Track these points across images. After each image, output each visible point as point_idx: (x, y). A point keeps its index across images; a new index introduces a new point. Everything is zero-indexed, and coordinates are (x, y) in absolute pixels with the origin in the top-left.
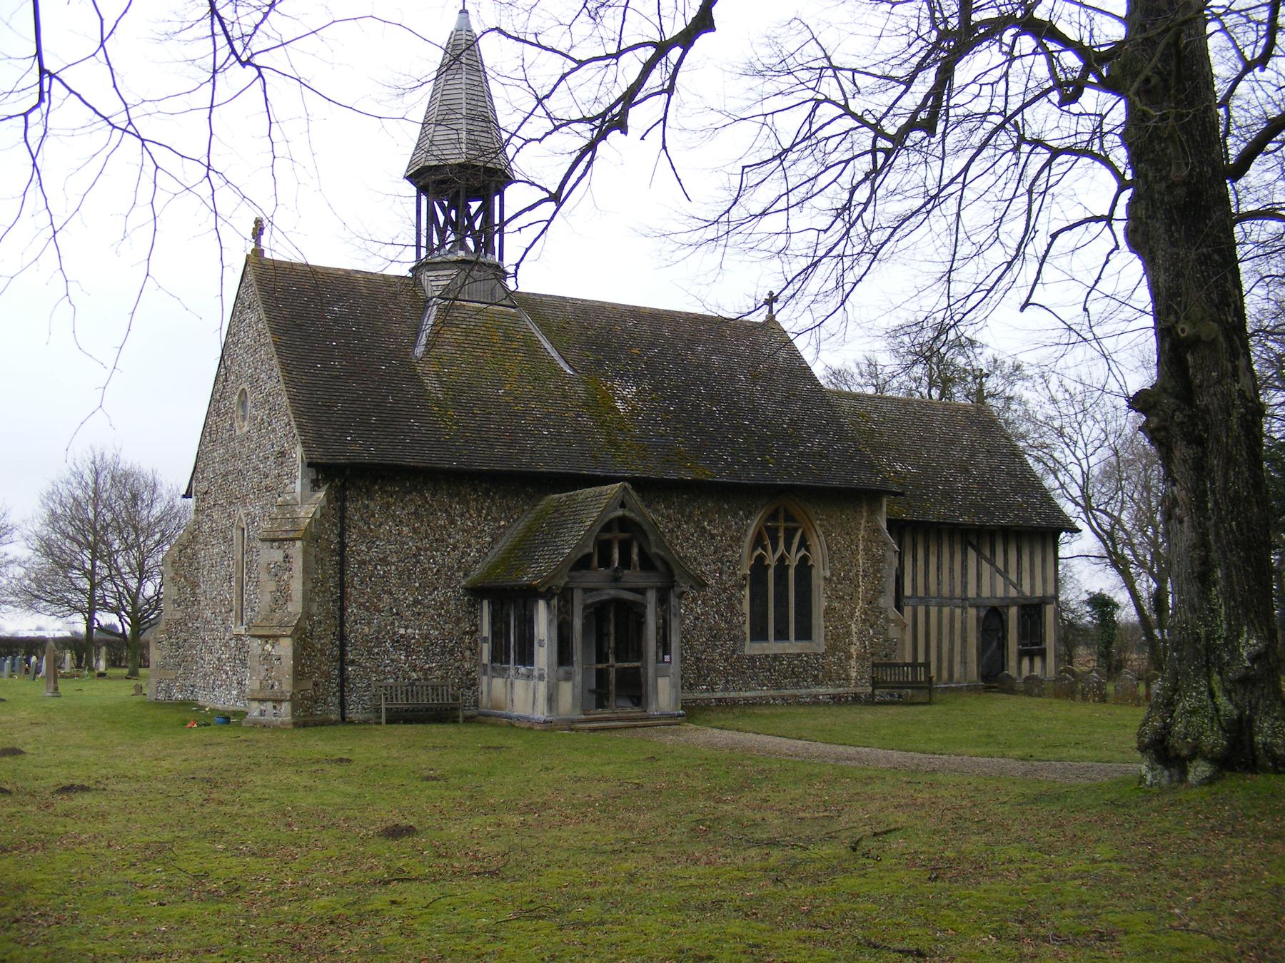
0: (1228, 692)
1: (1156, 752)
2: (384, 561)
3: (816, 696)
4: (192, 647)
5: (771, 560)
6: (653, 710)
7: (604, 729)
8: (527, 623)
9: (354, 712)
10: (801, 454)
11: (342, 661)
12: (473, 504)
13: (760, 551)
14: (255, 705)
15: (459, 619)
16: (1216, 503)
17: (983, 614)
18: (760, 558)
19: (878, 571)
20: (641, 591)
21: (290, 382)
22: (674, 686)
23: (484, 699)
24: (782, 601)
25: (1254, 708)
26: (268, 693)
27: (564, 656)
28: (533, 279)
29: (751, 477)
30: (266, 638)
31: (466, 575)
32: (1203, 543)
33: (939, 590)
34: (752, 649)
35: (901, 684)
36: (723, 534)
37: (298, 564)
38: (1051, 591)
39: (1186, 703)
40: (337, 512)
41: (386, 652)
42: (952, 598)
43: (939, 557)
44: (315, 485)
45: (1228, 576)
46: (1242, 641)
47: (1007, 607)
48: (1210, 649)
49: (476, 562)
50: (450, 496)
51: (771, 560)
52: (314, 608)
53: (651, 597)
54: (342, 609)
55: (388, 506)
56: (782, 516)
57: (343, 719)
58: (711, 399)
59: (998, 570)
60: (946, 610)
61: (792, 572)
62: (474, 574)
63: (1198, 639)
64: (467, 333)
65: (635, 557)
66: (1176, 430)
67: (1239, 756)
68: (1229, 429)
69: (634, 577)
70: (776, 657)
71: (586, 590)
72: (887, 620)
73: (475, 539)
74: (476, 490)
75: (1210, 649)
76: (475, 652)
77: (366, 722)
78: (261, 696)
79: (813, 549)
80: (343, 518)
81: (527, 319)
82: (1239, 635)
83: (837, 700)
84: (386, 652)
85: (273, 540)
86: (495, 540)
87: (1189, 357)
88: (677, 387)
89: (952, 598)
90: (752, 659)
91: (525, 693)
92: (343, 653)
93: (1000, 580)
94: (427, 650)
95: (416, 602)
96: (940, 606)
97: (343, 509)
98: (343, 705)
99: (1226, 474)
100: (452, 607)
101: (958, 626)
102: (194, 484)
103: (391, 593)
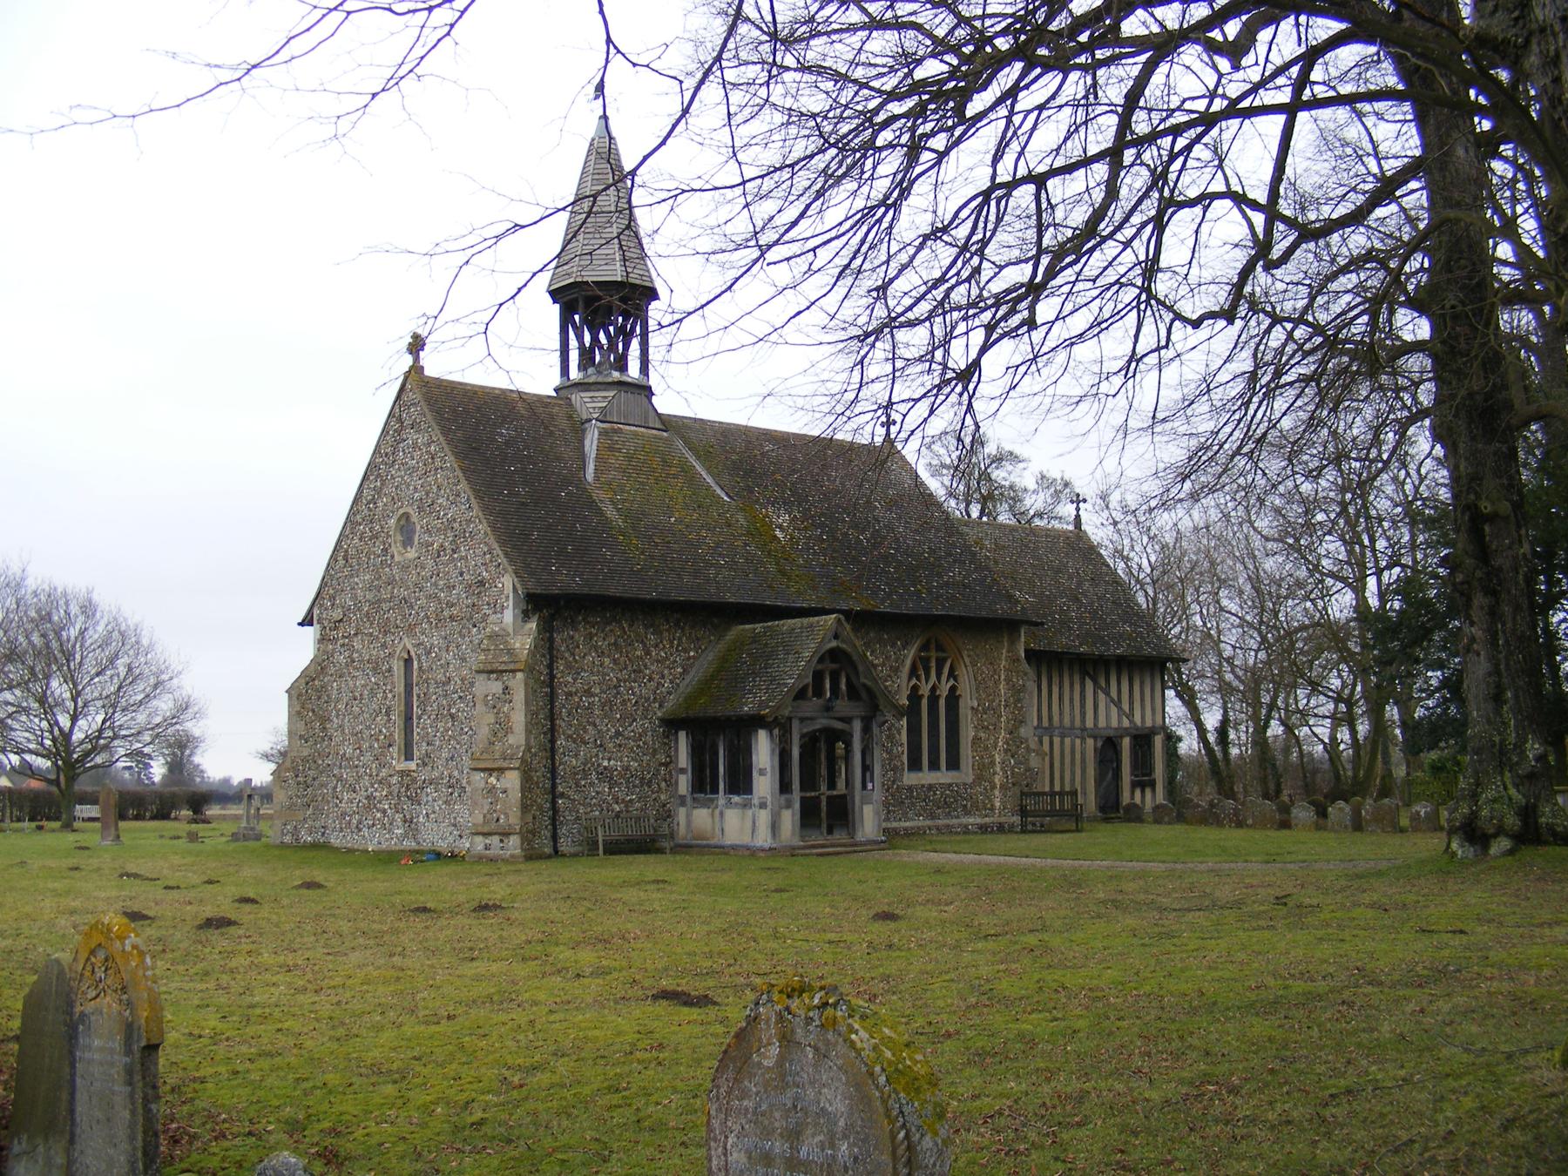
0: (1516, 786)
1: (1465, 833)
2: (588, 693)
3: (966, 826)
4: (322, 786)
5: (925, 690)
6: (860, 837)
7: (829, 854)
8: (748, 752)
9: (565, 845)
10: (947, 584)
11: (554, 795)
12: (666, 634)
13: (914, 681)
14: (479, 839)
15: (655, 750)
16: (1507, 641)
17: (1099, 744)
18: (915, 688)
19: (1019, 700)
20: (847, 720)
21: (485, 509)
22: (877, 813)
23: (682, 830)
24: (936, 734)
25: (1537, 798)
26: (493, 826)
27: (785, 787)
28: (666, 403)
29: (909, 608)
30: (490, 771)
31: (661, 706)
32: (1496, 672)
33: (1061, 720)
34: (910, 779)
35: (1043, 812)
36: (883, 665)
37: (519, 696)
38: (1159, 721)
39: (1490, 794)
40: (547, 646)
41: (592, 784)
42: (1072, 728)
43: (1072, 685)
44: (526, 615)
45: (1516, 697)
46: (1528, 746)
47: (1121, 737)
48: (1502, 752)
49: (669, 693)
50: (646, 627)
51: (925, 690)
52: (533, 742)
53: (857, 726)
54: (553, 741)
55: (591, 636)
56: (933, 646)
57: (556, 852)
58: (855, 526)
59: (1112, 701)
60: (1067, 741)
61: (942, 702)
62: (669, 704)
63: (1494, 746)
64: (630, 458)
65: (843, 687)
66: (1476, 583)
67: (1530, 834)
68: (1517, 583)
69: (843, 706)
70: (930, 787)
71: (802, 720)
72: (1028, 749)
73: (671, 670)
74: (668, 621)
75: (1502, 752)
76: (672, 784)
77: (575, 855)
78: (486, 829)
79: (961, 679)
80: (551, 649)
81: (680, 443)
82: (1526, 741)
83: (984, 829)
84: (592, 784)
85: (492, 672)
86: (685, 671)
87: (1487, 528)
88: (823, 514)
89: (1072, 728)
90: (910, 788)
91: (753, 819)
92: (554, 786)
93: (1114, 710)
94: (628, 782)
95: (618, 734)
96: (1063, 737)
97: (551, 640)
98: (555, 838)
99: (1514, 619)
100: (649, 739)
101: (1078, 756)
102: (316, 612)
103: (595, 725)
